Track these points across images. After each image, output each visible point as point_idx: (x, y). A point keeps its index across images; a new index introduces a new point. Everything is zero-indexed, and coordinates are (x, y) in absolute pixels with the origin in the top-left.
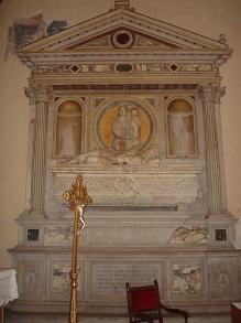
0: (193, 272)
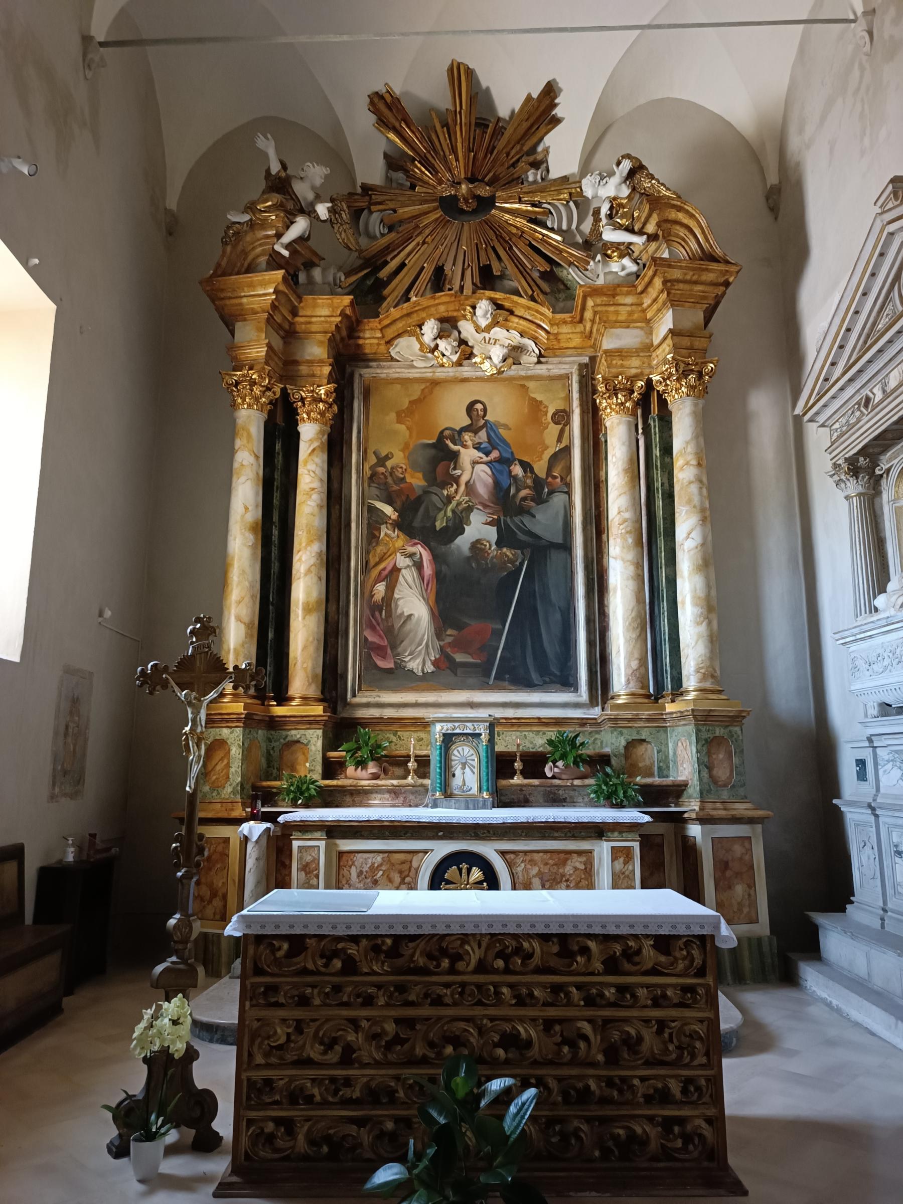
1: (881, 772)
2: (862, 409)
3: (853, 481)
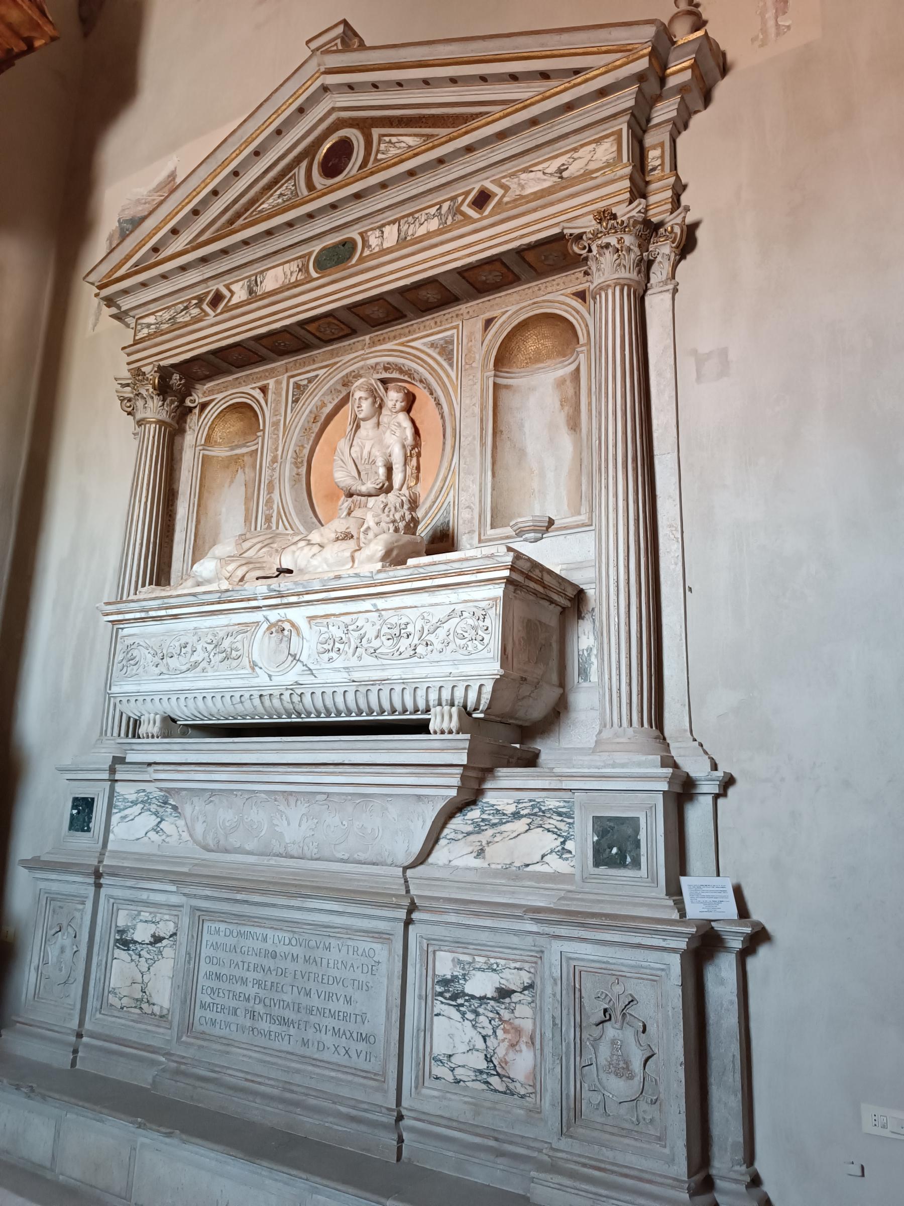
0: (503, 993)
1: (115, 819)
2: (205, 307)
3: (157, 402)
